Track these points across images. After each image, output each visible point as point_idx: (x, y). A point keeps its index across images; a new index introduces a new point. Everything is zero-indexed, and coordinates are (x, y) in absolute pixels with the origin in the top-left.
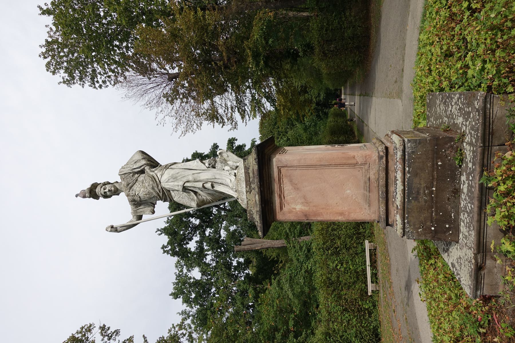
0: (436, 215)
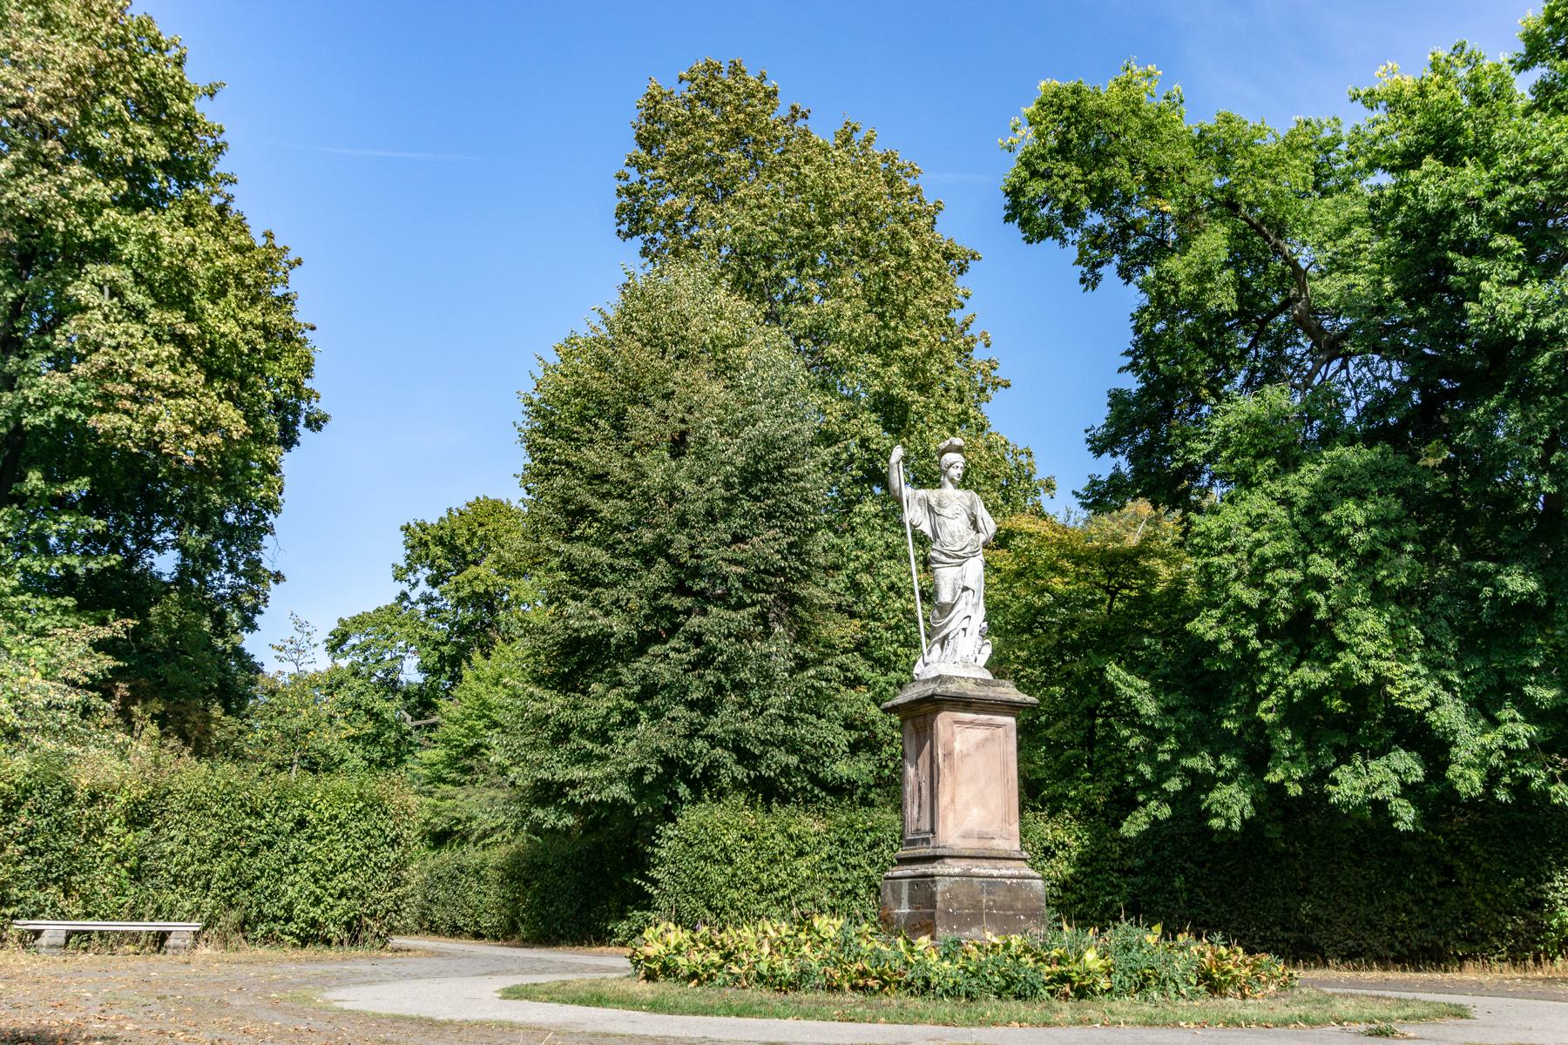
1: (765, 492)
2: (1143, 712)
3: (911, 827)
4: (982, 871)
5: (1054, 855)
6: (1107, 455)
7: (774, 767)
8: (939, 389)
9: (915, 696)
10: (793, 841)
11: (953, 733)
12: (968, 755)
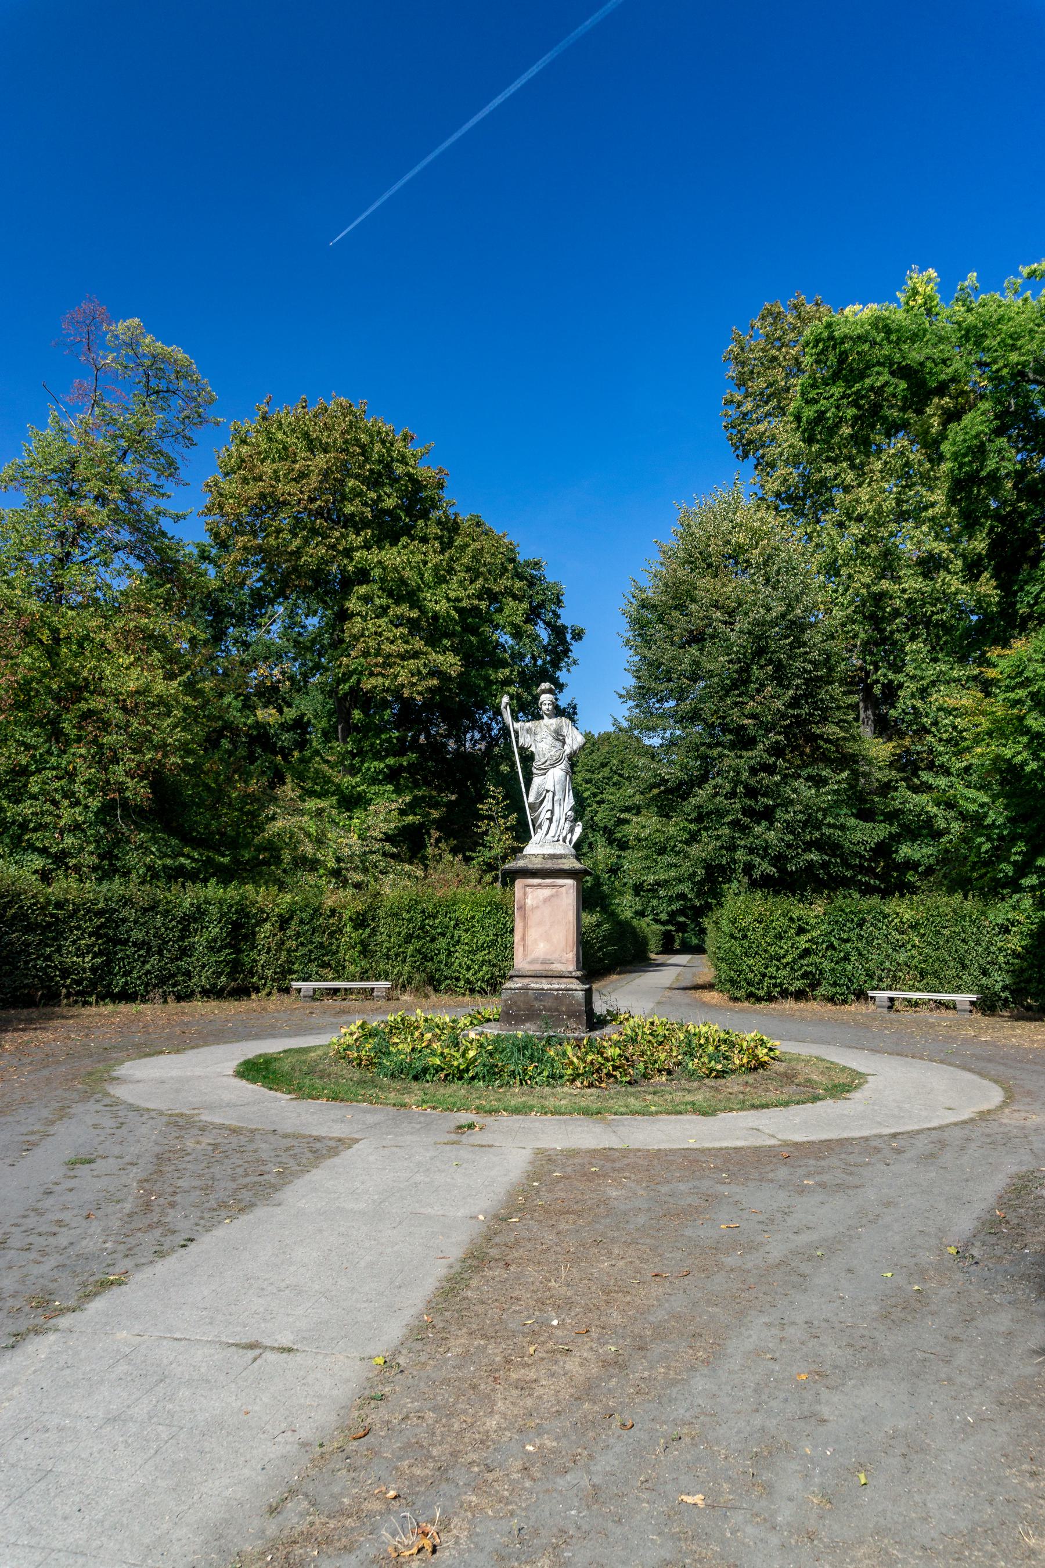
12: (537, 907)
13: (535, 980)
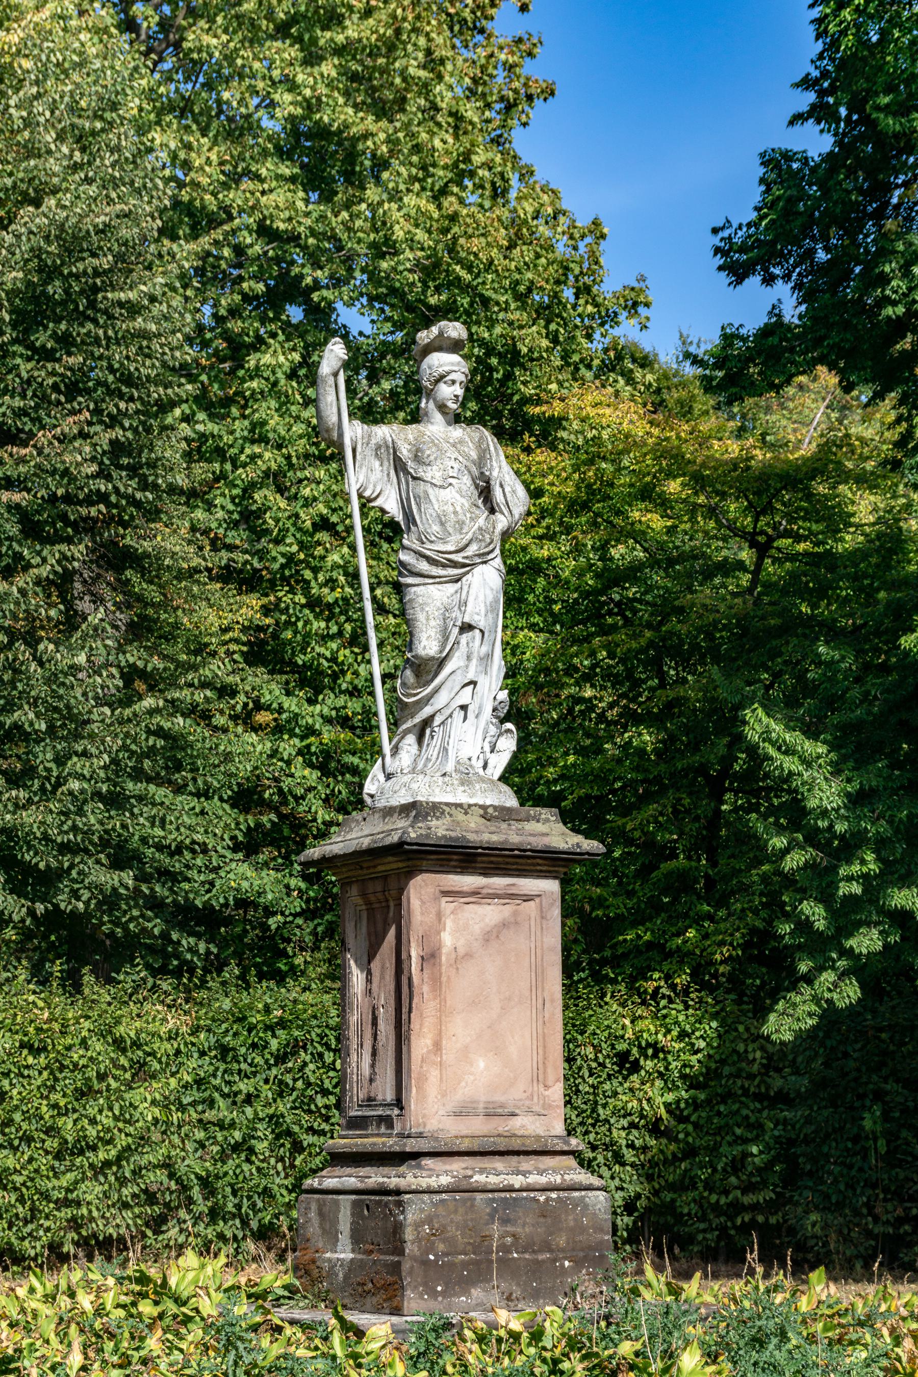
0: (463, 1261)
1: (66, 342)
2: (812, 803)
3: (356, 1093)
4: (493, 1180)
5: (636, 1067)
6: (754, 281)
7: (86, 895)
8: (413, 103)
9: (366, 843)
10: (124, 1051)
11: (439, 916)
12: (468, 955)
13: (486, 1162)
